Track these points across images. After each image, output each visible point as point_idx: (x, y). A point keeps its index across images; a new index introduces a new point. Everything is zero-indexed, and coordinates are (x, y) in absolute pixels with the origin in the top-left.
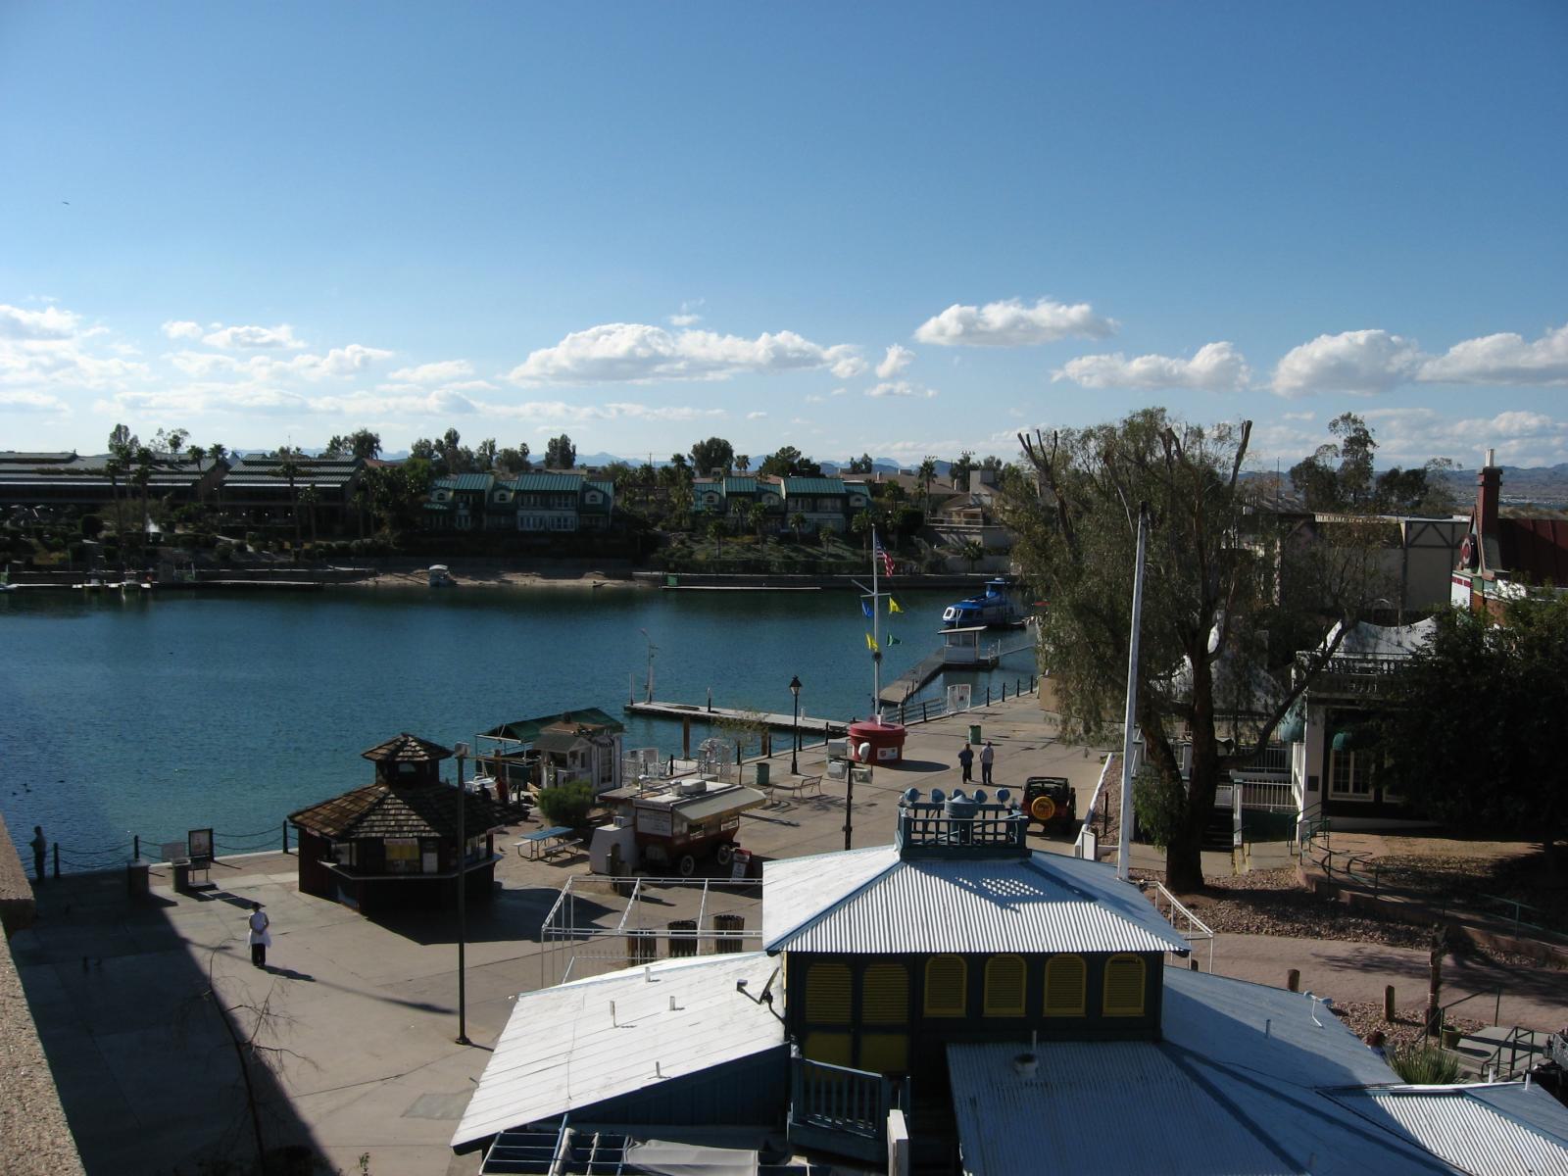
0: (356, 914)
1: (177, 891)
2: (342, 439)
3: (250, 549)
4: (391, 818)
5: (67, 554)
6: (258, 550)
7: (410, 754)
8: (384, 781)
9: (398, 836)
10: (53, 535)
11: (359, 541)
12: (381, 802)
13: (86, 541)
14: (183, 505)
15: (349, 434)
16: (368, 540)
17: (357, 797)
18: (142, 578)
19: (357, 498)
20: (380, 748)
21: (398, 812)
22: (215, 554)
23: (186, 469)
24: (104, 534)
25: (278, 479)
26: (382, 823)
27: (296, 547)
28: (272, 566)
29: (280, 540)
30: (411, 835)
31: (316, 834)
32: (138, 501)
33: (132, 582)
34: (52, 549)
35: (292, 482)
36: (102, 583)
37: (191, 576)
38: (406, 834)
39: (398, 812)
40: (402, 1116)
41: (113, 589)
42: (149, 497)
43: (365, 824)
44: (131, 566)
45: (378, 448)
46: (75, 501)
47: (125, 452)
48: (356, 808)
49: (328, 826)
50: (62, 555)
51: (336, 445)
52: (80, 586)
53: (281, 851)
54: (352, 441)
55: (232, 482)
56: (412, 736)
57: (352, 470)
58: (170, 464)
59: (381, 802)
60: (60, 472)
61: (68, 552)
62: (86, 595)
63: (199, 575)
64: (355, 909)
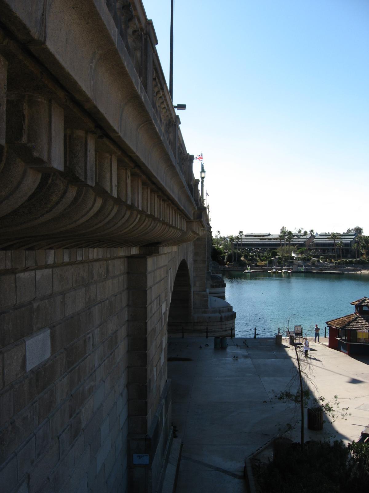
0: (347, 355)
1: (290, 344)
2: (351, 229)
3: (321, 261)
4: (360, 323)
5: (266, 262)
6: (324, 262)
7: (367, 303)
8: (358, 312)
9: (361, 329)
10: (263, 256)
11: (355, 259)
12: (356, 318)
13: (272, 259)
14: (301, 248)
15: (353, 228)
16: (358, 259)
17: (349, 317)
18: (288, 269)
19: (355, 245)
20: (357, 301)
21: (362, 322)
22: (310, 263)
23: (302, 237)
24: (277, 257)
25: (330, 240)
26: (356, 325)
27: (336, 261)
28: (328, 266)
29: (331, 259)
30: (366, 329)
31: (335, 327)
32: (288, 247)
33: (285, 270)
34: (262, 261)
35: (334, 241)
36: (276, 270)
37: (303, 269)
38: (364, 329)
39: (362, 322)
40: (356, 409)
41: (280, 272)
42: (291, 245)
43: (351, 325)
44: (285, 266)
45: (362, 232)
46: (270, 247)
47: (286, 235)
48: (348, 320)
49: (338, 325)
50: (265, 262)
51: (349, 231)
52: (270, 271)
53: (324, 337)
54: (354, 230)
55: (316, 241)
56: (367, 298)
57: (353, 237)
58: (297, 236)
59: (356, 318)
60: (266, 239)
61: (267, 261)
62: (272, 274)
63: (305, 269)
64: (346, 354)
